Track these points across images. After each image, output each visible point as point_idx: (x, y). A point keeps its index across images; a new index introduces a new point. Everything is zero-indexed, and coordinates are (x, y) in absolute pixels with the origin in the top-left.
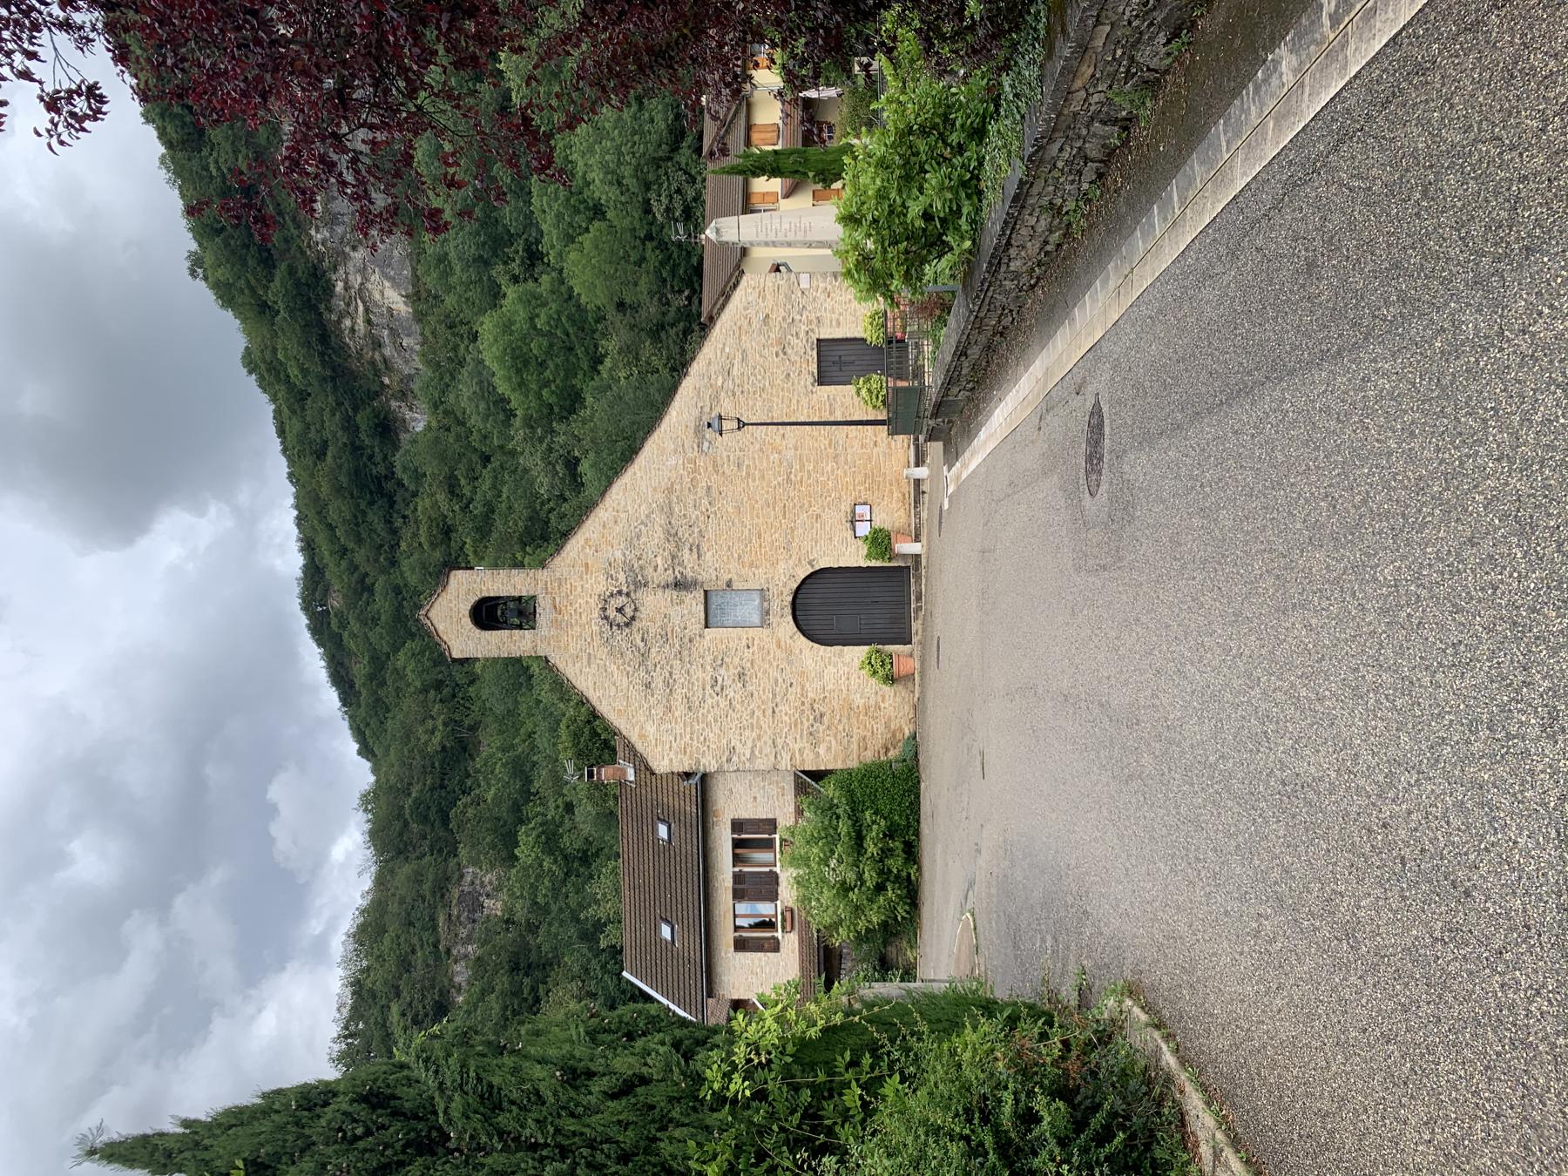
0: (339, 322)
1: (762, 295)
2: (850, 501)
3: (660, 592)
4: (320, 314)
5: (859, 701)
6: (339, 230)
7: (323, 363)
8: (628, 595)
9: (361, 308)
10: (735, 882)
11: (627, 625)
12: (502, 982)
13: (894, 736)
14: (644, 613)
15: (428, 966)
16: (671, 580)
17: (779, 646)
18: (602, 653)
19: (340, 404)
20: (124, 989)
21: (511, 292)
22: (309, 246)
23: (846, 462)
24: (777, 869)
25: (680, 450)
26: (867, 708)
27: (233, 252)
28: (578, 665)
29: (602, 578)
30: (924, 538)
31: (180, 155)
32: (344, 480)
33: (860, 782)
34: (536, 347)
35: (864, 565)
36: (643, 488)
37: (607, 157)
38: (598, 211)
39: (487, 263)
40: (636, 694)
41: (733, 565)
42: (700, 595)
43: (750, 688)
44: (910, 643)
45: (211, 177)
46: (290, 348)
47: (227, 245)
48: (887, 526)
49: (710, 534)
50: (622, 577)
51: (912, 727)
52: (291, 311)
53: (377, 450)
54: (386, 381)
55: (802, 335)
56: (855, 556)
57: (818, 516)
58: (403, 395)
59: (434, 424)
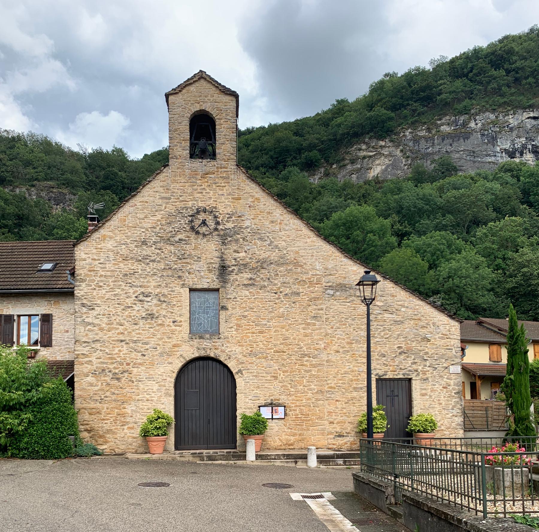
0: (364, 143)
1: (445, 336)
2: (287, 402)
3: (217, 254)
4: (368, 133)
5: (129, 409)
6: (411, 144)
7: (343, 134)
8: (216, 229)
9: (371, 154)
10: (6, 316)
11: (192, 228)
12: (10, 209)
13: (101, 437)
14: (202, 242)
15: (26, 175)
16: (228, 263)
17: (175, 346)
18: (171, 208)
19: (322, 142)
21: (387, 222)
22: (402, 128)
23: (317, 400)
24: (15, 347)
25: (328, 273)
26: (123, 415)
27: (399, 91)
28: (161, 190)
29: (229, 210)
30: (259, 463)
31: (447, 66)
32: (284, 144)
33: (58, 410)
34: (357, 234)
35: (239, 413)
36: (298, 244)
37: (464, 271)
38: (433, 266)
39: (399, 212)
40: (138, 234)
41: (238, 312)
42: (215, 285)
43: (141, 322)
44: (177, 448)
45: (436, 81)
46: (351, 118)
47: (403, 88)
48: (268, 432)
49: (262, 294)
50: (230, 225)
51: (107, 451)
52: (369, 118)
53: (299, 161)
54: (334, 166)
55: (414, 367)
56: (245, 406)
57: (276, 378)
58: (327, 175)
59: (313, 186)
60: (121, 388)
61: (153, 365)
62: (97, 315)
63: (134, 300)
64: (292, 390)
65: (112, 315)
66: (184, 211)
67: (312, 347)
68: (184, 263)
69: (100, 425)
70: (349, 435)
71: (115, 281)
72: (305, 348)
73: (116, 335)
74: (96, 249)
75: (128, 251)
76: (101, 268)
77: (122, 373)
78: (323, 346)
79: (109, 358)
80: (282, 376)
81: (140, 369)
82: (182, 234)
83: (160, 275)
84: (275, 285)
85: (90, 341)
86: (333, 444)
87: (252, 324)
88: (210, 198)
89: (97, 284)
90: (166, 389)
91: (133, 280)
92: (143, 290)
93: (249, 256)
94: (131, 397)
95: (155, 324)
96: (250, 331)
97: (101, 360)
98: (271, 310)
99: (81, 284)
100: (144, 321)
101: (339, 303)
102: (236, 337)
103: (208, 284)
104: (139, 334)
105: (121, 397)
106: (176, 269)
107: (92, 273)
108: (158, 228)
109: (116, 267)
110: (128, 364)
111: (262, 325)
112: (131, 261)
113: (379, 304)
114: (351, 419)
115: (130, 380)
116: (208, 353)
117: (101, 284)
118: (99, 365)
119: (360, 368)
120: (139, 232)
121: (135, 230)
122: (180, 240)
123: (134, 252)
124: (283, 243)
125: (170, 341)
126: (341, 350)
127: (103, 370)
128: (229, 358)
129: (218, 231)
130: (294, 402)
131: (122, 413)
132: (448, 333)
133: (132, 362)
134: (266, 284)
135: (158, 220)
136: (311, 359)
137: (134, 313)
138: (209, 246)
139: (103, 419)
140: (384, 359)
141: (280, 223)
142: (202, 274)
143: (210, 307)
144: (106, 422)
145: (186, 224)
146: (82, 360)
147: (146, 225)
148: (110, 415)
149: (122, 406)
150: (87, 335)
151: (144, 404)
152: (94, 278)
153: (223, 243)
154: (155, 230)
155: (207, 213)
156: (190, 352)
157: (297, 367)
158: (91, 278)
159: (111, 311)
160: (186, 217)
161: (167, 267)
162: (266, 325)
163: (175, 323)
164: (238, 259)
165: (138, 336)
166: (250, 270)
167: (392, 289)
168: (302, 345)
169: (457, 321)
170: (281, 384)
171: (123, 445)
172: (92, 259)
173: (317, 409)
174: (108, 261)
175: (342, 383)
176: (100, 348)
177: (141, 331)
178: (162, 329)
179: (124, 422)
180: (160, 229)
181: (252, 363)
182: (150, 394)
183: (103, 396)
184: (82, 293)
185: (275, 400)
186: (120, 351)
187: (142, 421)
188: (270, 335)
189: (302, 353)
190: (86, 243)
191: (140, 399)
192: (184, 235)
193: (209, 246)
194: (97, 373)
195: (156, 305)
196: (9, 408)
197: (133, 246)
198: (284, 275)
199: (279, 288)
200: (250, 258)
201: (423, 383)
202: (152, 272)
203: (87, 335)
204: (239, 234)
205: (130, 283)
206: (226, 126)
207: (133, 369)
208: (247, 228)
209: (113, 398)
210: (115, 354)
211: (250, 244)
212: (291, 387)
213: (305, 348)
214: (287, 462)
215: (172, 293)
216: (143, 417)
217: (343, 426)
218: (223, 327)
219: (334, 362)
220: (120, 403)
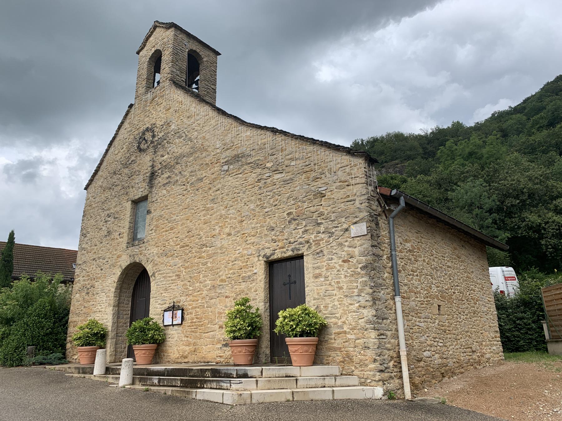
8: (152, 142)
20: (424, 79)
55: (306, 236)
78: (217, 231)
80: (184, 273)
101: (232, 178)
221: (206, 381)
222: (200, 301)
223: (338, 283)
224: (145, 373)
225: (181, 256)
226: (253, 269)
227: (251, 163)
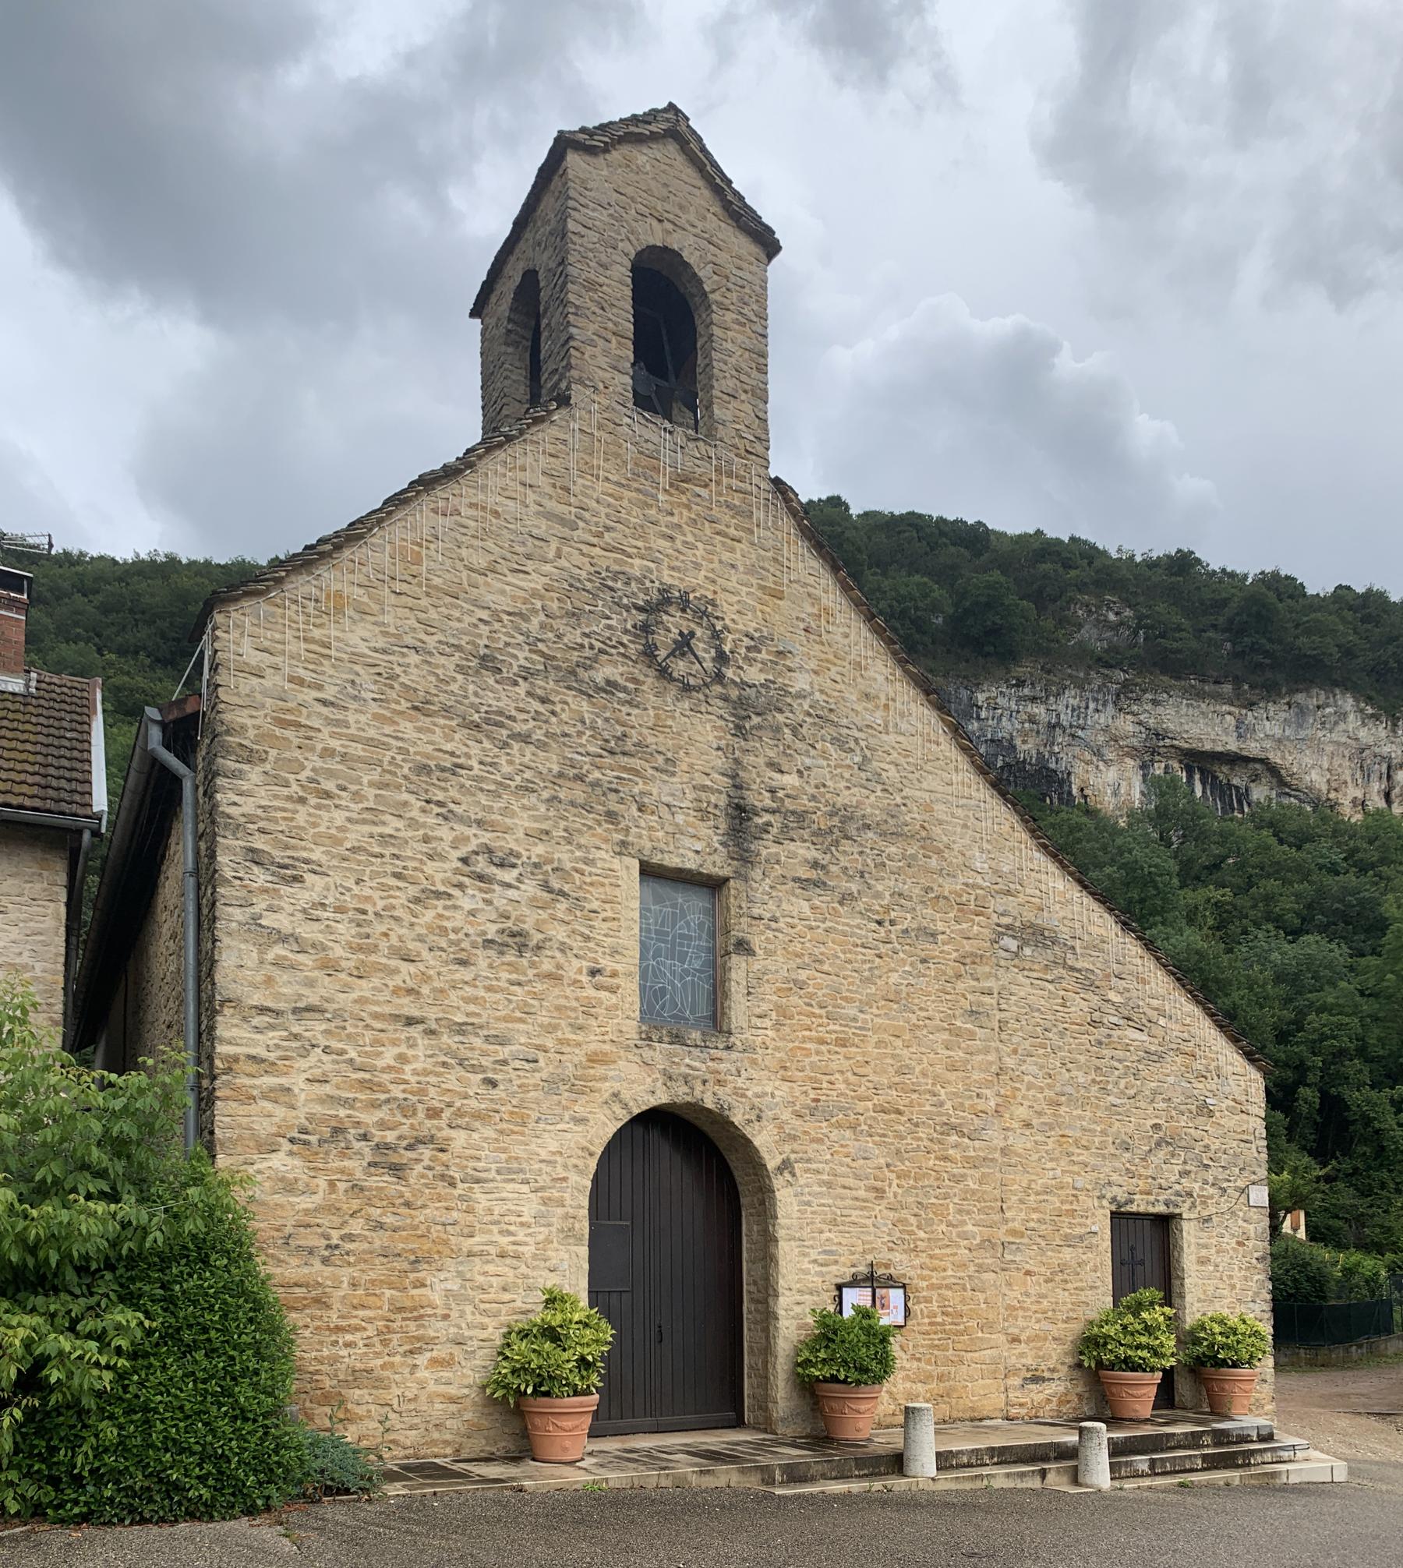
5: (438, 1286)
13: (326, 1398)
16: (752, 799)
17: (594, 1059)
18: (575, 562)
23: (981, 1269)
26: (416, 1312)
42: (717, 864)
43: (483, 959)
50: (754, 675)
57: (880, 1193)
60: (408, 1205)
61: (524, 1124)
62: (314, 906)
63: (457, 871)
64: (922, 1234)
65: (371, 917)
66: (619, 585)
67: (967, 1103)
68: (625, 769)
69: (326, 1352)
70: (1056, 1376)
71: (385, 786)
72: (948, 1105)
73: (386, 995)
74: (305, 640)
75: (433, 679)
76: (329, 722)
77: (410, 1147)
78: (992, 1104)
79: (361, 1082)
80: (894, 1188)
81: (475, 1136)
82: (615, 663)
83: (546, 795)
84: (878, 895)
85: (281, 1006)
86: (1021, 1405)
87: (817, 1011)
88: (697, 566)
89: (311, 780)
90: (566, 1216)
91: (453, 793)
92: (486, 837)
93: (811, 790)
94: (446, 1242)
95: (531, 972)
96: (813, 1033)
97: (327, 1089)
98: (866, 974)
99: (246, 767)
100: (492, 953)
101: (1028, 981)
102: (777, 1049)
103: (698, 859)
104: (474, 1000)
105: (405, 1240)
106: (596, 784)
107: (289, 733)
108: (535, 621)
109: (388, 730)
110: (434, 1113)
111: (846, 1018)
112: (442, 721)
113: (1115, 999)
114: (1056, 1330)
115: (443, 1177)
116: (697, 1093)
117: (330, 786)
118: (318, 1109)
119: (1076, 1177)
120: (467, 619)
121: (457, 607)
122: (608, 682)
123: (454, 687)
124: (892, 771)
125: (580, 1038)
126: (1035, 1122)
127: (338, 1131)
128: (759, 1118)
129: (724, 686)
130: (925, 1272)
131: (408, 1304)
132: (1243, 1098)
133: (449, 1105)
134: (854, 888)
135: (534, 594)
136: (966, 1140)
137: (458, 919)
138: (700, 728)
139: (339, 1329)
140: (1127, 1155)
141: (886, 706)
142: (680, 818)
143: (690, 938)
144: (349, 1337)
145: (626, 632)
146: (247, 1081)
147: (493, 597)
148: (361, 1313)
149: (412, 1276)
150: (269, 981)
151: (490, 1268)
152: (297, 753)
153: (738, 727)
154: (524, 625)
155: (689, 615)
156: (646, 1091)
157: (931, 1163)
158: (287, 755)
159: (368, 899)
160: (627, 609)
161: (572, 772)
162: (855, 1019)
163: (598, 978)
164: (781, 794)
165: (472, 1008)
166: (814, 834)
167: (1139, 961)
168: (943, 1097)
169: (1259, 1069)
170: (891, 1214)
171: (411, 1428)
172: (291, 680)
173: (981, 1297)
174: (355, 698)
175: (1039, 1221)
176: (323, 1042)
177: (482, 993)
178: (555, 995)
179: (418, 1339)
180: (543, 626)
181: (819, 1141)
182: (510, 1233)
183: (335, 1236)
184: (248, 806)
185: (880, 1265)
186: (402, 1058)
187: (484, 1335)
188: (864, 1054)
189: (944, 1119)
190: (263, 607)
191: (476, 1249)
192: (621, 669)
193: (700, 728)
194: (313, 1139)
195: (535, 904)
196: (20, 1279)
197: (450, 664)
198: (897, 872)
199: (888, 909)
200: (813, 798)
201: (1202, 1230)
202: (518, 778)
203: (269, 981)
204: (780, 711)
205: (440, 804)
206: (740, 338)
207: (453, 1133)
208: (801, 695)
209: (377, 1244)
210: (383, 1071)
211: (813, 752)
212: (919, 1227)
213: (948, 1105)
214: (1022, 1475)
215: (587, 869)
216: (486, 1320)
217: (1040, 1349)
218: (739, 1010)
219: (1019, 1155)
220: (406, 1266)
221: (1253, 1452)
222: (950, 1273)
223: (1231, 1277)
224: (1052, 1455)
225: (884, 1135)
226: (1088, 1222)
227: (1079, 971)
